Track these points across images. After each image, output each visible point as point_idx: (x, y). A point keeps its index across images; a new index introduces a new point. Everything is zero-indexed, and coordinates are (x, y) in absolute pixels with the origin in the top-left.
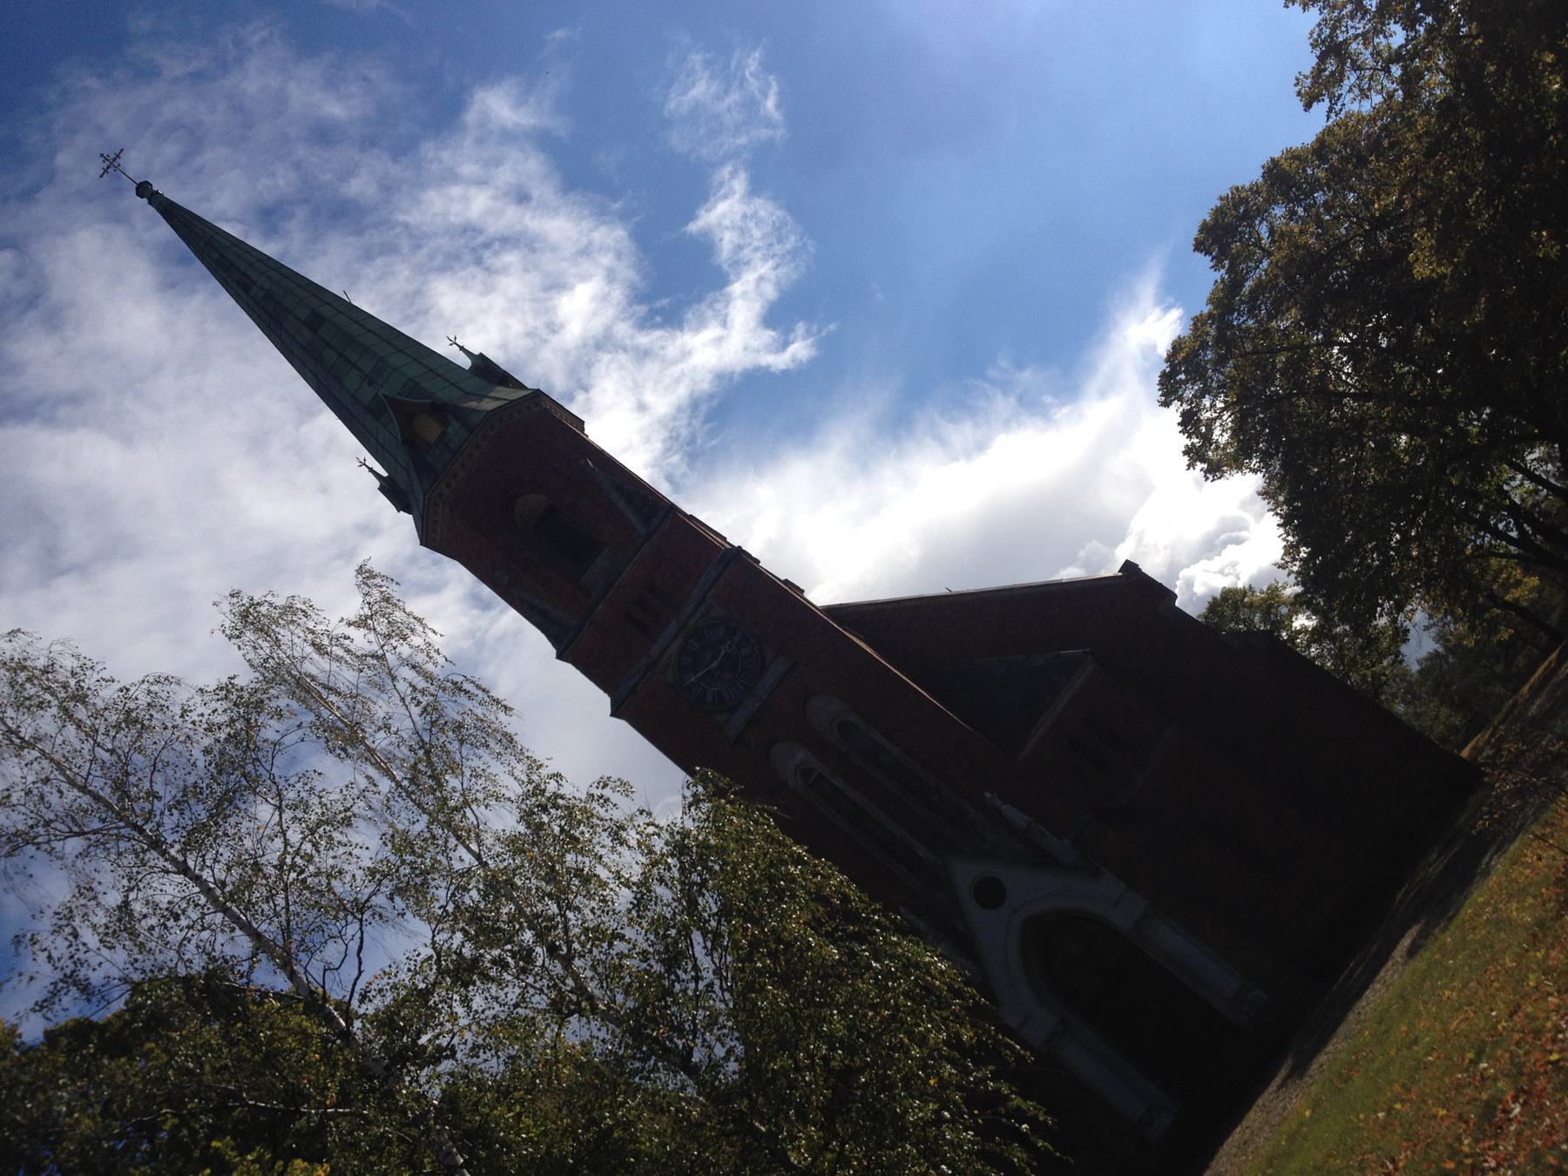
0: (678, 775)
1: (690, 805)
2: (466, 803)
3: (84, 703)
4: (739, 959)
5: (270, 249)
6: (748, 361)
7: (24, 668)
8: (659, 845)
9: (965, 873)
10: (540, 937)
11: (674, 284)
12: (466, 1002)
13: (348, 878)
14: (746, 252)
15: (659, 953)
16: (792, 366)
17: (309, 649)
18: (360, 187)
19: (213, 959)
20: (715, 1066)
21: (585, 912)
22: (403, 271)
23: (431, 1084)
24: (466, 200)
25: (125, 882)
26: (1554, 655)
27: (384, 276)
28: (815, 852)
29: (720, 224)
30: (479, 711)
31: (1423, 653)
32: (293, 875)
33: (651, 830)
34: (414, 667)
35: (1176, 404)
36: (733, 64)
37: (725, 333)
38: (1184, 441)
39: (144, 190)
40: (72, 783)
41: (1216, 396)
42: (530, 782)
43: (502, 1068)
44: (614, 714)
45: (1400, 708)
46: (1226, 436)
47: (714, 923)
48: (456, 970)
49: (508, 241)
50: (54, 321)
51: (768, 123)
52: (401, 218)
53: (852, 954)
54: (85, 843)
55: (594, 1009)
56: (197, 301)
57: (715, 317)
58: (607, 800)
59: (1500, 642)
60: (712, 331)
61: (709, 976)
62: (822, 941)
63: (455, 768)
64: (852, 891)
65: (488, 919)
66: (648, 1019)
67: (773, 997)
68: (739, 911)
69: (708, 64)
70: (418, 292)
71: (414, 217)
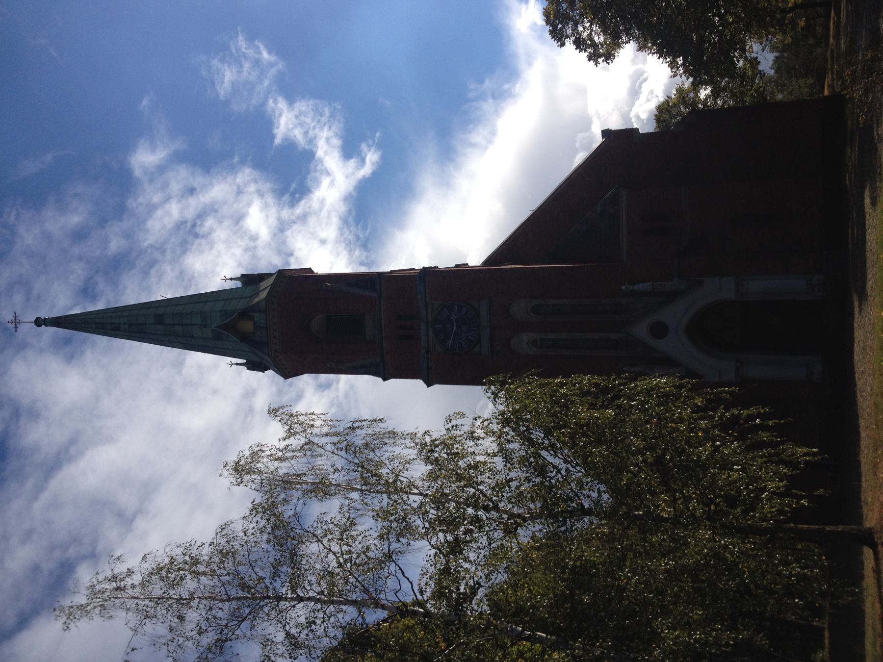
0: (478, 390)
1: (494, 399)
2: (397, 476)
3: (200, 563)
4: (570, 449)
5: (100, 306)
6: (353, 181)
7: (161, 569)
8: (495, 427)
9: (641, 330)
10: (476, 507)
11: (290, 175)
12: (466, 560)
13: (373, 547)
14: (311, 133)
15: (533, 473)
16: (374, 168)
17: (276, 463)
18: (116, 245)
19: (343, 628)
20: (597, 503)
21: (486, 482)
22: (167, 268)
23: (480, 605)
24: (168, 213)
25: (280, 625)
26: (833, 14)
27: (160, 278)
28: (566, 375)
29: (288, 129)
30: (370, 431)
31: (771, 63)
32: (349, 565)
33: (486, 423)
34: (326, 435)
35: (567, 41)
36: (234, 51)
37: (332, 178)
38: (584, 55)
39: (39, 322)
40: (222, 601)
41: (583, 22)
42: (417, 444)
43: (505, 575)
44: (429, 386)
45: (780, 96)
46: (602, 37)
47: (546, 442)
48: (451, 550)
49: (201, 216)
50: (34, 414)
51: (271, 65)
52: (145, 244)
53: (619, 407)
54: (249, 621)
55: (525, 520)
56: (89, 355)
57: (321, 174)
58: (456, 426)
59: (802, 29)
60: (325, 182)
61: (563, 466)
62: (601, 411)
63: (381, 464)
64: (596, 379)
65: (447, 517)
66: (551, 505)
67: (599, 452)
68: (554, 427)
69: (222, 60)
70: (182, 272)
71: (150, 240)
